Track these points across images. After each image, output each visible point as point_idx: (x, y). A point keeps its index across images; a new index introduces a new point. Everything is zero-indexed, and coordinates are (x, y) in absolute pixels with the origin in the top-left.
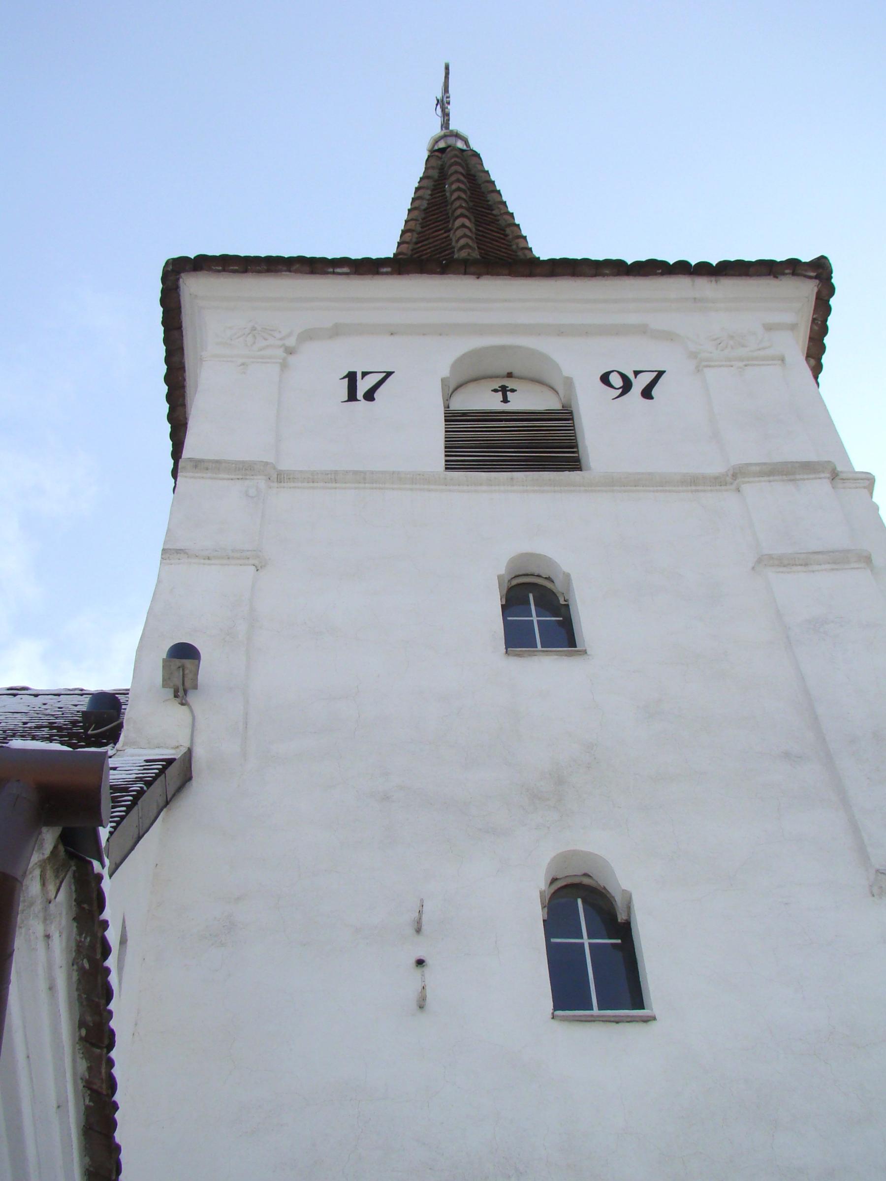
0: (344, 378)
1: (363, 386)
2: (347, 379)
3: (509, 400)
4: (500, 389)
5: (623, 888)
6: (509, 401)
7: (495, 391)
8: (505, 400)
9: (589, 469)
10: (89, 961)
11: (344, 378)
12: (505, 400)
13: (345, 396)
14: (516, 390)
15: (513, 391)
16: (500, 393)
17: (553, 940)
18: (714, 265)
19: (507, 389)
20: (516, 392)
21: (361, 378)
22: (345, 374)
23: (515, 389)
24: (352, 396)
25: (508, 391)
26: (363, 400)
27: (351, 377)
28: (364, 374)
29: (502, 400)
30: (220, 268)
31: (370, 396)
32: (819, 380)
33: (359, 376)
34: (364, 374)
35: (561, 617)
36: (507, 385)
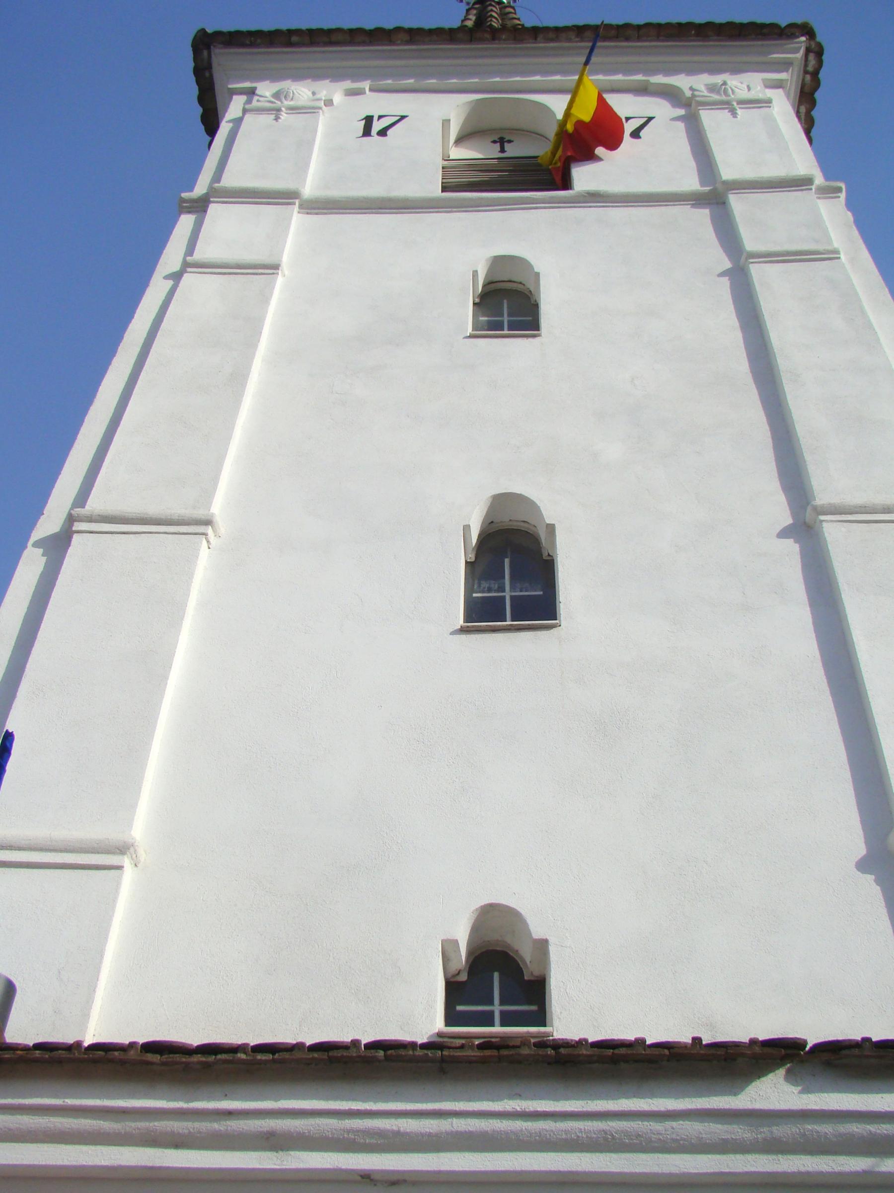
0: (363, 120)
1: (377, 126)
2: (364, 121)
3: (506, 150)
4: (498, 140)
5: (548, 522)
6: (506, 151)
7: (494, 142)
8: (502, 150)
9: (574, 189)
10: (37, 1050)
11: (363, 120)
12: (502, 150)
13: (361, 133)
14: (513, 141)
15: (510, 141)
16: (498, 144)
17: (534, 1008)
18: (727, 278)
19: (505, 140)
20: (512, 143)
21: (377, 119)
22: (364, 116)
23: (512, 140)
24: (367, 132)
25: (506, 141)
26: (376, 135)
27: (369, 120)
28: (380, 117)
29: (499, 150)
30: (562, 1050)
31: (383, 133)
32: (812, 134)
33: (375, 118)
34: (380, 117)
35: (530, 317)
36: (504, 137)
